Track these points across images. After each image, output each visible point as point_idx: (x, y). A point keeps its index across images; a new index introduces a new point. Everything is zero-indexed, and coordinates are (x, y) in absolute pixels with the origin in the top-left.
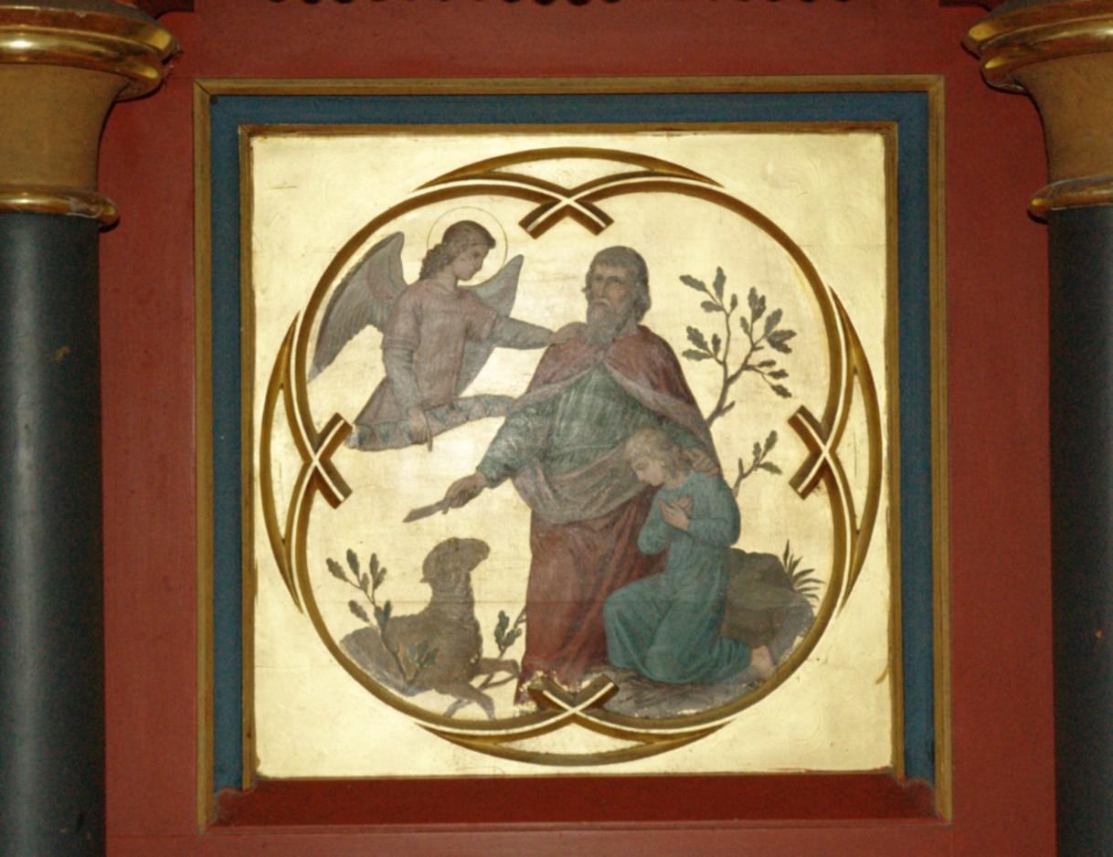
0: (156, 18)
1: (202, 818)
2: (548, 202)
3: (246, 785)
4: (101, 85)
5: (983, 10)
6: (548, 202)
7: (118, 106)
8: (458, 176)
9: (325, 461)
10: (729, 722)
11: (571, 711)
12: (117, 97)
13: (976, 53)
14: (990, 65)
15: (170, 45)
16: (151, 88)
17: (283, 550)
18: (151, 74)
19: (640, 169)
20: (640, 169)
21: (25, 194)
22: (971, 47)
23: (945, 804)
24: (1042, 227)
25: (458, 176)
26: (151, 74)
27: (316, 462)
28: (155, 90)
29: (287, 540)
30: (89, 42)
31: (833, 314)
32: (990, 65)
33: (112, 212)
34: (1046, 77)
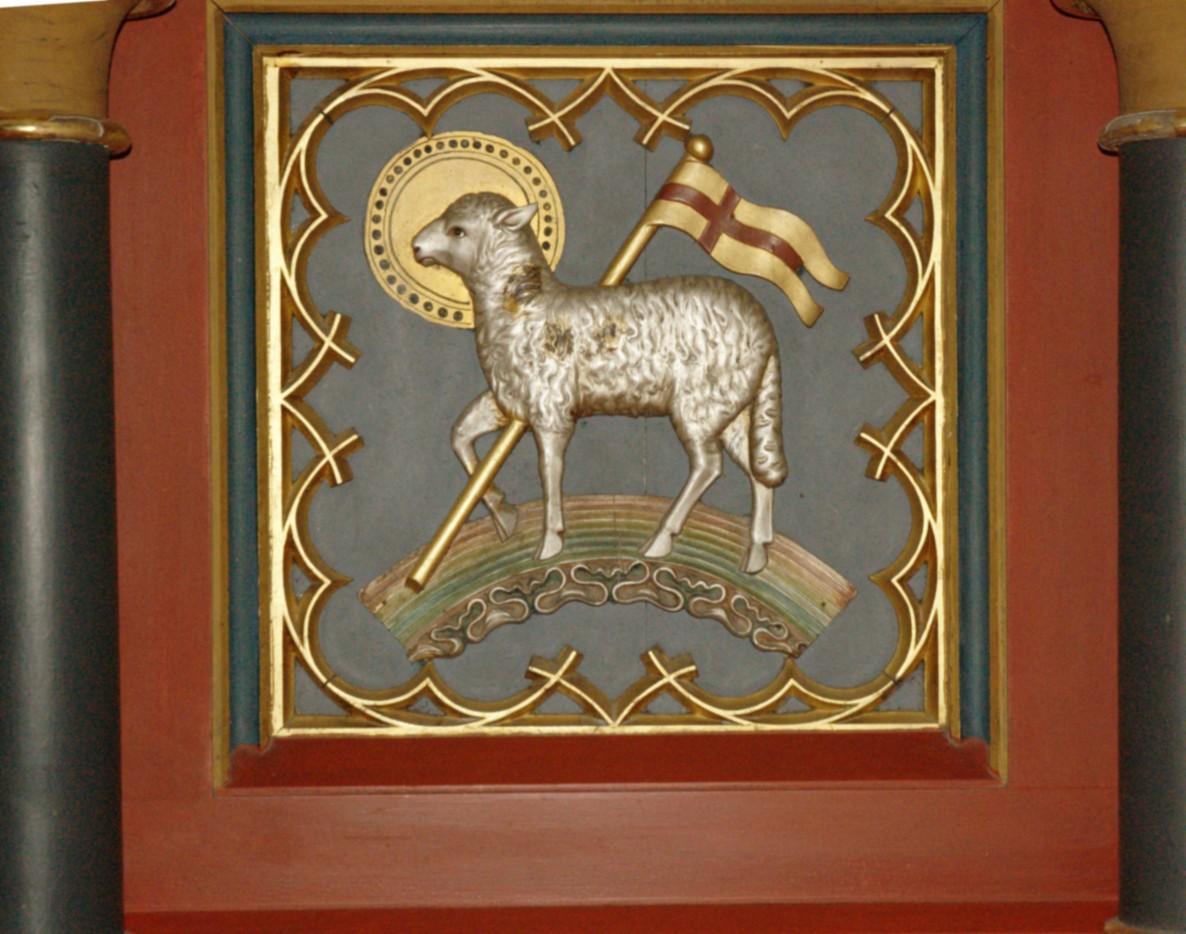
3: (263, 743)
7: (128, 25)
12: (128, 14)
23: (1001, 759)
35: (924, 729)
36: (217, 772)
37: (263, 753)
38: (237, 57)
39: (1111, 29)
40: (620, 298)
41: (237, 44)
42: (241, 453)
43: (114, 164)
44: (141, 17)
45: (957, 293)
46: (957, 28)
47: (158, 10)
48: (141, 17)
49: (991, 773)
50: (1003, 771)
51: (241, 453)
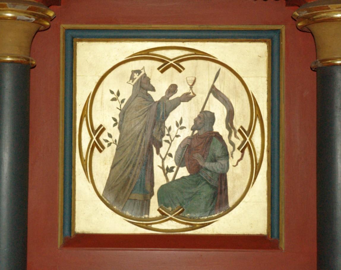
0: (48, 7)
1: (59, 246)
2: (248, 133)
3: (72, 235)
4: (34, 27)
5: (298, 7)
6: (248, 133)
7: (38, 33)
8: (255, 100)
9: (171, 65)
10: (217, 221)
11: (170, 216)
12: (38, 30)
13: (295, 19)
14: (299, 24)
15: (53, 16)
16: (48, 27)
17: (85, 163)
18: (48, 24)
19: (85, 119)
20: (85, 119)
21: (8, 57)
22: (294, 17)
23: (283, 245)
24: (315, 73)
25: (255, 100)
26: (48, 24)
27: (94, 139)
28: (47, 28)
29: (86, 160)
30: (27, 14)
31: (168, 66)
32: (299, 24)
33: (34, 63)
34: (316, 28)
35: (268, 151)
36: (60, 241)
37: (72, 238)
38: (69, 43)
39: (316, 39)
40: (338, 85)
41: (69, 39)
42: (276, 95)
43: (32, 70)
44: (42, 31)
45: (271, 135)
46: (272, 34)
47: (46, 29)
48: (42, 31)
49: (280, 248)
50: (284, 249)
51: (276, 95)
